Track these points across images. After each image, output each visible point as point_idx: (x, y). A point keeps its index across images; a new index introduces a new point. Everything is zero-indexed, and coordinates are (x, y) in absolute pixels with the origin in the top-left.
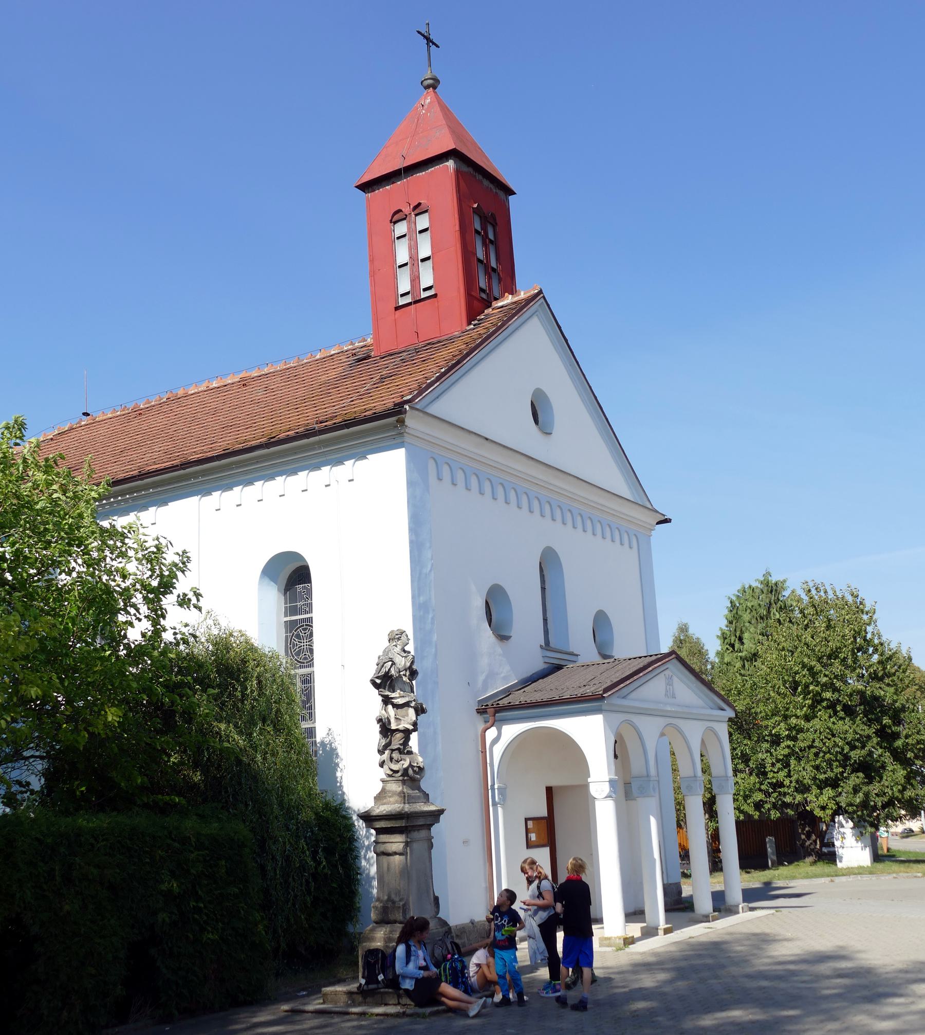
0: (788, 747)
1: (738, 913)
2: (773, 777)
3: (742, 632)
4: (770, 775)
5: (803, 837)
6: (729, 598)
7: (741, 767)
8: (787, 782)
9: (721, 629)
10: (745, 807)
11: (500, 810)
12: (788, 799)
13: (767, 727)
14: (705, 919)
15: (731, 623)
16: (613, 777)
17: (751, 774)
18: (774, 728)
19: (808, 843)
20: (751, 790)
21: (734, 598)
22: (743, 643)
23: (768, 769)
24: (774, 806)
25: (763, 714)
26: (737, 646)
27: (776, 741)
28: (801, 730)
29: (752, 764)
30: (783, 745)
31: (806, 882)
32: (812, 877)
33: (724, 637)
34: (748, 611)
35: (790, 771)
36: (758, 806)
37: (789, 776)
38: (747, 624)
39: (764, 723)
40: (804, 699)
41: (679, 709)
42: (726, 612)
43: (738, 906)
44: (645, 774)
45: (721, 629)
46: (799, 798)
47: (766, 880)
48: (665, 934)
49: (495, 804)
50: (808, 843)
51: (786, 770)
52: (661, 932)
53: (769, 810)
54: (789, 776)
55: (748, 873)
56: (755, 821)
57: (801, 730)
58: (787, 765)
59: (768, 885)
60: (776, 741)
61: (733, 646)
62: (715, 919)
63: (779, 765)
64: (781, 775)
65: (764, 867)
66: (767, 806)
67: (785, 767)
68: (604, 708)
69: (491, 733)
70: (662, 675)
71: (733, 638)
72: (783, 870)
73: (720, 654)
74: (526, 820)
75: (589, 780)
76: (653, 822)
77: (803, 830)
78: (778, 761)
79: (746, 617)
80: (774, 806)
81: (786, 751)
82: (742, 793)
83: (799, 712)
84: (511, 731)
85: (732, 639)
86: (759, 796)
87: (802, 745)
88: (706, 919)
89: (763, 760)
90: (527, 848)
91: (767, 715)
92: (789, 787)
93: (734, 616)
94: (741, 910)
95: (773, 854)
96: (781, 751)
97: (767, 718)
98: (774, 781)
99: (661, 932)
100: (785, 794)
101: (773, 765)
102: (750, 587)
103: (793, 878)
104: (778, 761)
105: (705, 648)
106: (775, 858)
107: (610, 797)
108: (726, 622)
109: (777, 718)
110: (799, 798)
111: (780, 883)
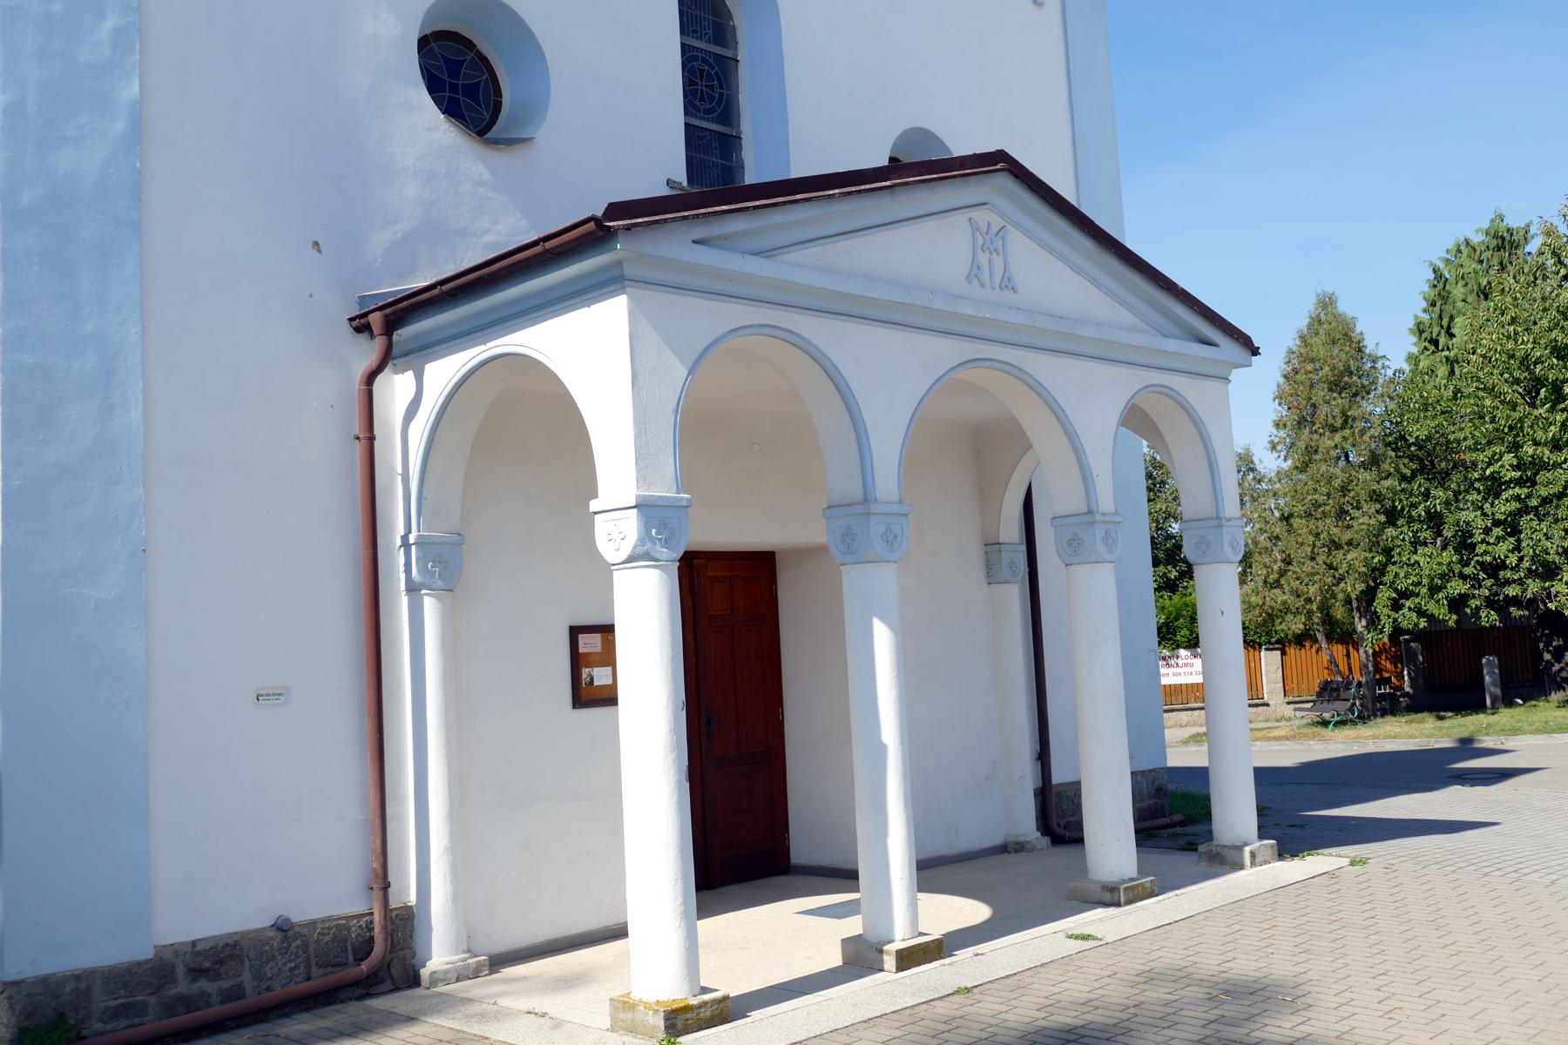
0: (1518, 498)
1: (1242, 867)
2: (1486, 553)
3: (1452, 318)
4: (1480, 549)
5: (1547, 656)
6: (1431, 264)
7: (1426, 535)
8: (1512, 560)
9: (1416, 317)
10: (1432, 607)
11: (429, 604)
12: (1512, 591)
13: (1474, 464)
14: (1107, 897)
15: (1433, 304)
16: (664, 490)
17: (1444, 548)
18: (1490, 464)
19: (1556, 667)
20: (1442, 576)
21: (1441, 265)
22: (1452, 336)
23: (1478, 538)
24: (1490, 603)
25: (1470, 442)
26: (1442, 341)
27: (1495, 487)
28: (1545, 466)
29: (1448, 533)
30: (1504, 495)
31: (1539, 740)
32: (1553, 731)
33: (1420, 329)
34: (1461, 283)
35: (1519, 541)
36: (1457, 604)
37: (1518, 548)
38: (1460, 304)
39: (1468, 457)
40: (1552, 410)
41: (1019, 319)
42: (1426, 288)
43: (1239, 848)
44: (859, 496)
45: (1416, 317)
46: (1534, 587)
47: (1464, 734)
48: (900, 968)
49: (412, 588)
50: (1556, 667)
51: (1512, 540)
52: (890, 962)
53: (1478, 609)
54: (1518, 548)
55: (1441, 718)
56: (1451, 629)
57: (1545, 466)
58: (1515, 531)
59: (1467, 747)
60: (1495, 487)
61: (1435, 342)
62: (1137, 895)
63: (1498, 531)
64: (1502, 549)
65: (1477, 706)
66: (1474, 603)
67: (1510, 535)
68: (628, 271)
69: (396, 388)
70: (960, 219)
71: (1436, 330)
72: (1505, 716)
73: (1413, 359)
74: (575, 632)
75: (594, 505)
76: (883, 639)
77: (1548, 644)
78: (1497, 523)
79: (1458, 292)
80: (1490, 603)
81: (1515, 505)
82: (1425, 581)
83: (1540, 435)
84: (444, 372)
85: (1433, 334)
86: (1457, 587)
87: (1544, 492)
88: (1111, 896)
89: (1468, 523)
90: (574, 707)
91: (1477, 443)
92: (1515, 569)
93: (1440, 295)
94: (1247, 860)
95: (1493, 683)
96: (1503, 508)
97: (1475, 448)
98: (1488, 559)
99: (890, 962)
100: (1508, 582)
101: (1487, 531)
102: (1467, 243)
103: (1515, 731)
104: (1497, 523)
105: (1359, 329)
106: (1499, 692)
107: (646, 556)
108: (1424, 304)
109: (1497, 449)
110: (1534, 587)
111: (1488, 742)
